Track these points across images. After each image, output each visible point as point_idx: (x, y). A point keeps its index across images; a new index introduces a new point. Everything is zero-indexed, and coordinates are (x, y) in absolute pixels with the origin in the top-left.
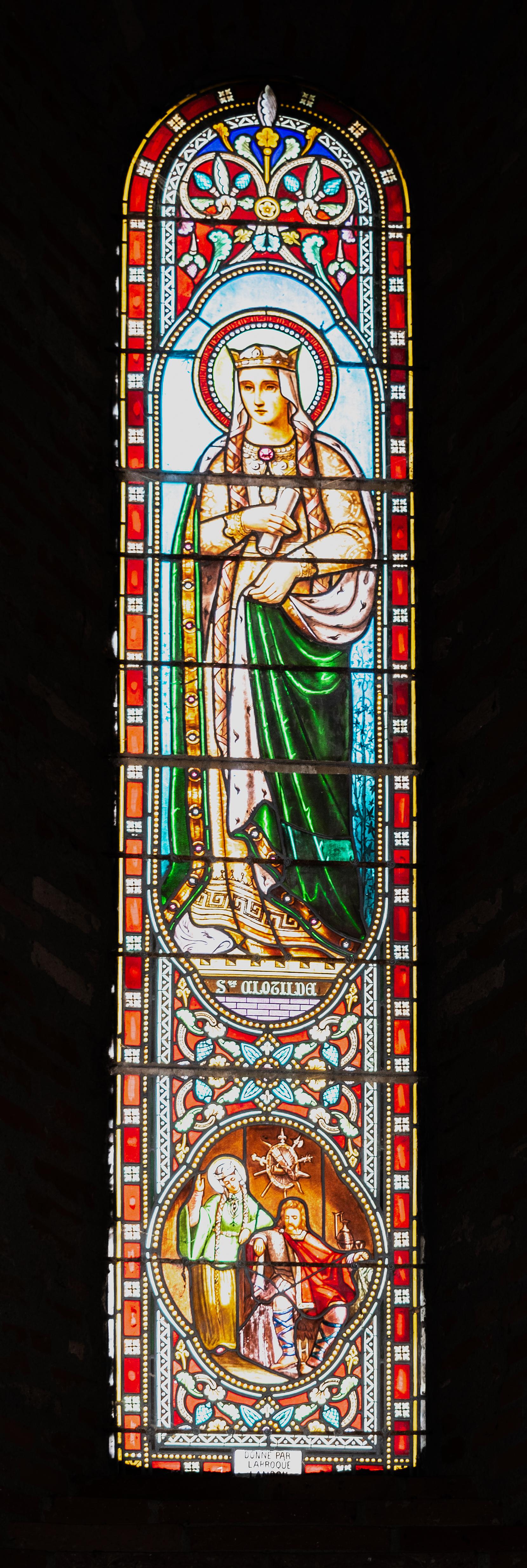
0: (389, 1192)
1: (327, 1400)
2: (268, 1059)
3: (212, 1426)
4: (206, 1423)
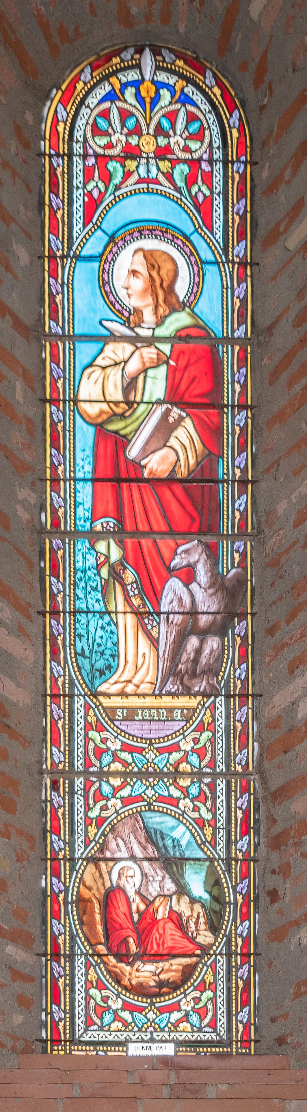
3: (114, 1026)
4: (109, 1025)
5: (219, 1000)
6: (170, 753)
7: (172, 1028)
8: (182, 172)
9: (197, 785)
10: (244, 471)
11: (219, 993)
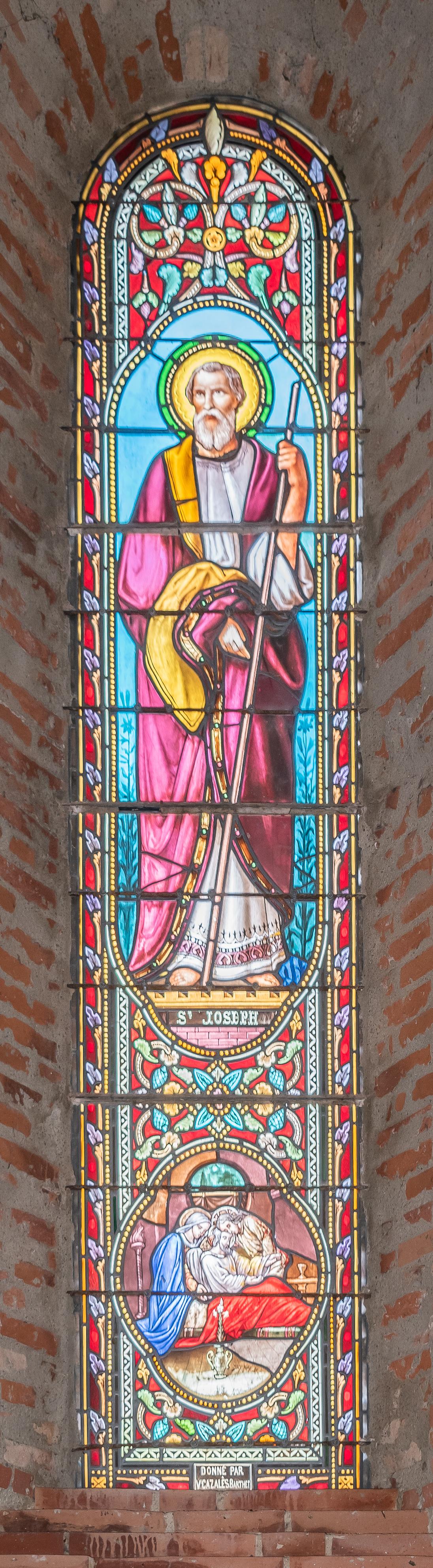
1: (275, 1414)
2: (219, 1113)
5: (313, 1404)
8: (259, 278)
9: (281, 1113)
10: (345, 792)
11: (312, 1394)
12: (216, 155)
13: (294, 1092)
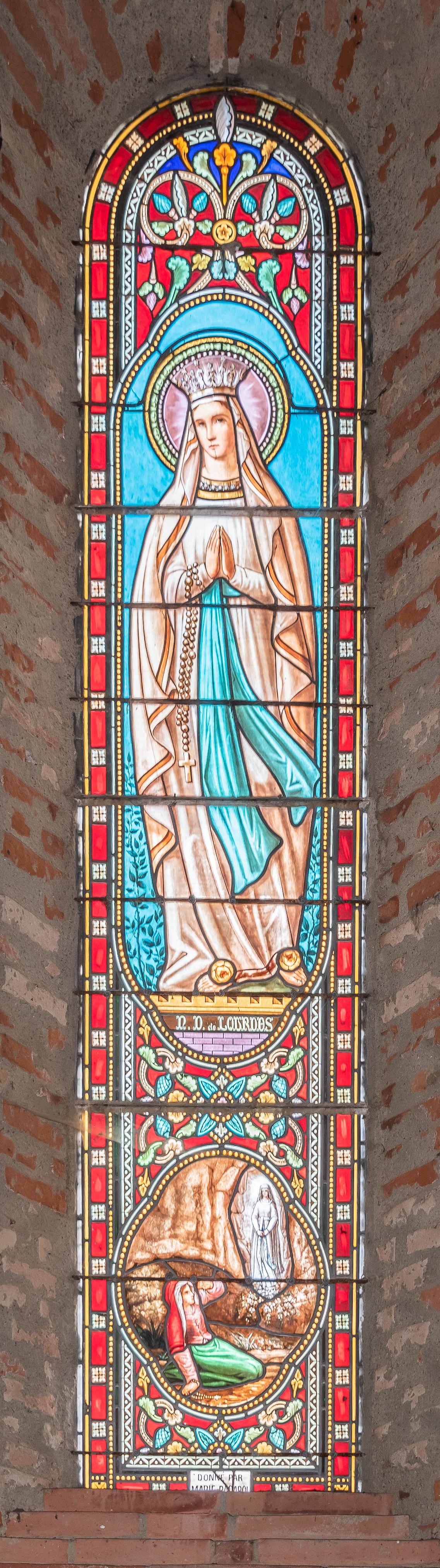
0: (332, 1052)
2: (219, 1444)
5: (310, 1414)
6: (248, 1077)
7: (247, 1450)
12: (226, 142)
13: (297, 1101)
